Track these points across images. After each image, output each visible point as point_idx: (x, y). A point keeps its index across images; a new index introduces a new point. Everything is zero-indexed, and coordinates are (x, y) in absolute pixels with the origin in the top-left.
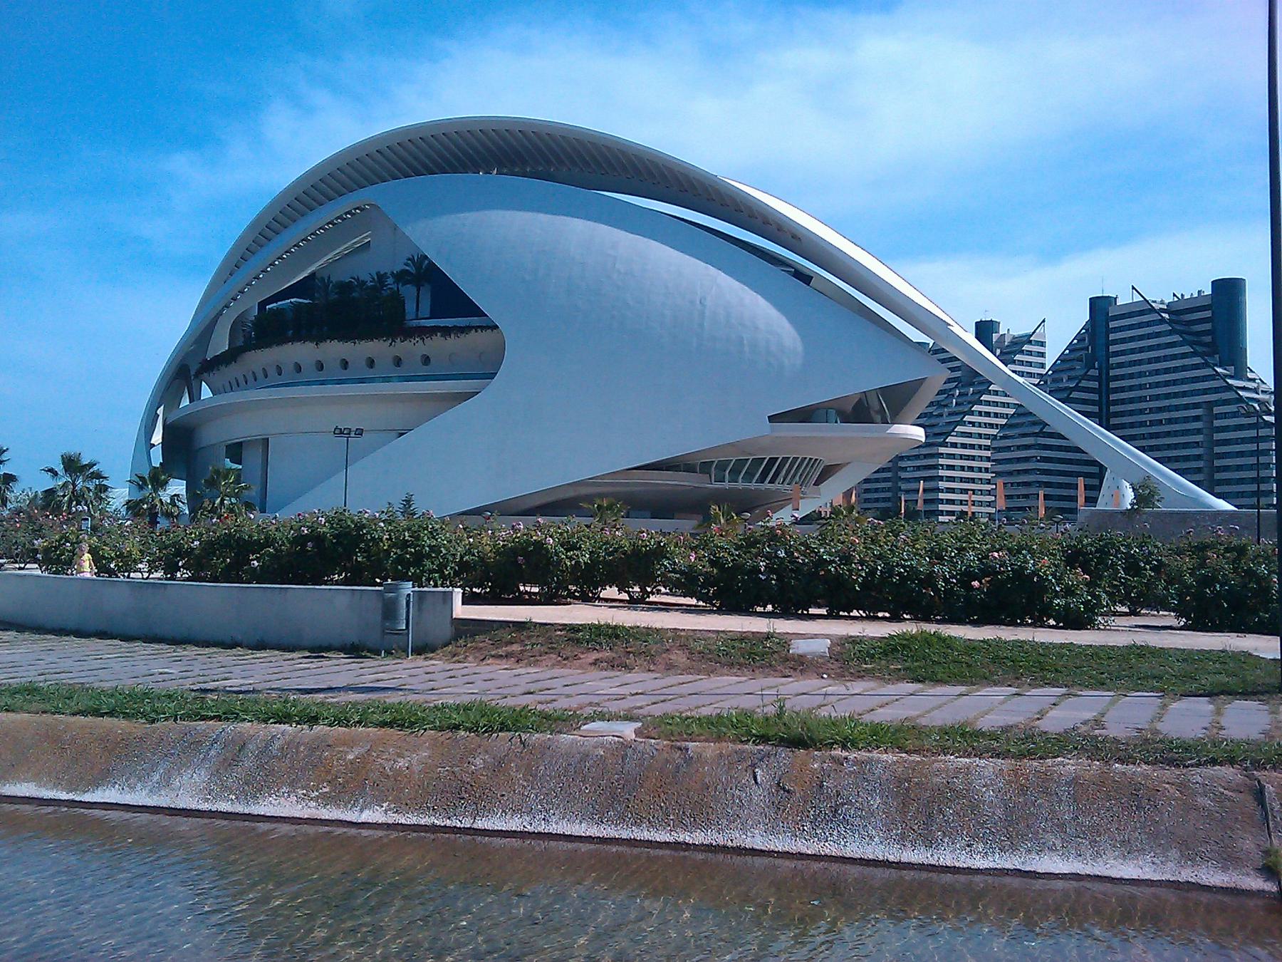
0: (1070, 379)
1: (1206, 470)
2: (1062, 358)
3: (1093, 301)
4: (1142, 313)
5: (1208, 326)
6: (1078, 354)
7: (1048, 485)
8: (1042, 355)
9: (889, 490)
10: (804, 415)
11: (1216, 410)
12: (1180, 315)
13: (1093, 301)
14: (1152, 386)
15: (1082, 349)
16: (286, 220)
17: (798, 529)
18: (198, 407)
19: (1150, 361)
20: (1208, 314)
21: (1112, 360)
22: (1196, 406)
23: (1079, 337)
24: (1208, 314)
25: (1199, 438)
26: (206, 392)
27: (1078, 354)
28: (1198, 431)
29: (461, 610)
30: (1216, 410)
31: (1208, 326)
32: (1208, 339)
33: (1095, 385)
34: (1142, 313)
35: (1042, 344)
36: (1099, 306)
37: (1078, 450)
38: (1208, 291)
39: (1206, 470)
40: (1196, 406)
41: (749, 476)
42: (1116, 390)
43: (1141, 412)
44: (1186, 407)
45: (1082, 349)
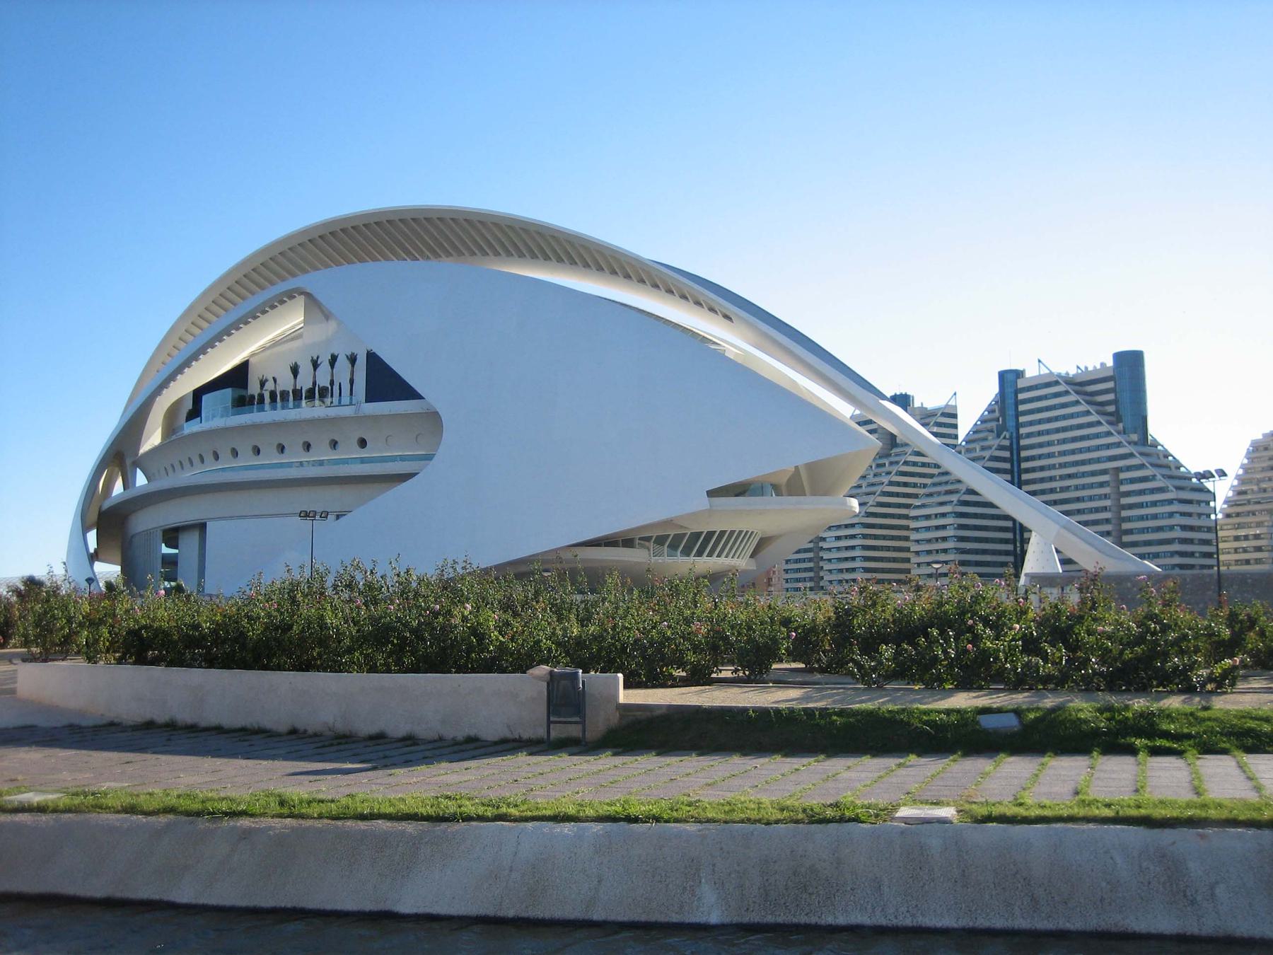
0: (983, 449)
1: (1113, 521)
2: (975, 430)
3: (1003, 376)
4: (1048, 385)
5: (1111, 397)
6: (989, 425)
7: (978, 564)
8: (955, 426)
9: (810, 560)
10: (739, 490)
11: (1123, 476)
12: (1081, 385)
13: (1003, 376)
14: (1062, 478)
15: (991, 420)
16: (215, 308)
17: (1227, 745)
18: (131, 493)
19: (1058, 430)
20: (1110, 385)
21: (1023, 442)
22: (1104, 472)
23: (990, 410)
24: (1110, 385)
25: (1108, 503)
26: (141, 479)
27: (989, 425)
28: (1106, 496)
29: (626, 696)
30: (1123, 476)
31: (1111, 397)
32: (1111, 409)
33: (1007, 454)
34: (1048, 385)
35: (955, 416)
36: (1009, 379)
37: (991, 505)
38: (1110, 363)
39: (1114, 509)
40: (1104, 472)
41: (687, 552)
42: (1028, 459)
43: (1051, 479)
44: (1093, 474)
45: (991, 420)
